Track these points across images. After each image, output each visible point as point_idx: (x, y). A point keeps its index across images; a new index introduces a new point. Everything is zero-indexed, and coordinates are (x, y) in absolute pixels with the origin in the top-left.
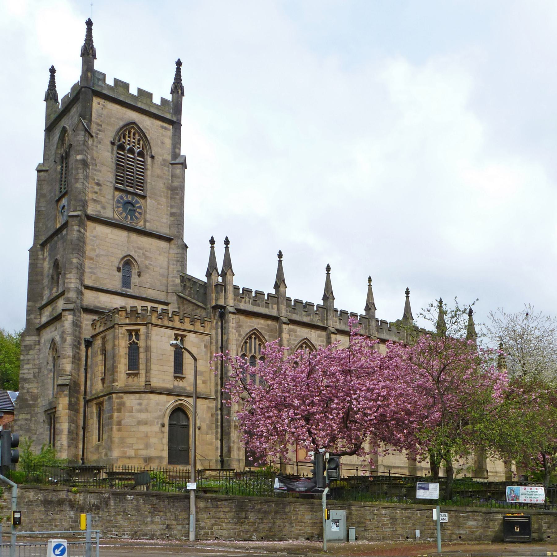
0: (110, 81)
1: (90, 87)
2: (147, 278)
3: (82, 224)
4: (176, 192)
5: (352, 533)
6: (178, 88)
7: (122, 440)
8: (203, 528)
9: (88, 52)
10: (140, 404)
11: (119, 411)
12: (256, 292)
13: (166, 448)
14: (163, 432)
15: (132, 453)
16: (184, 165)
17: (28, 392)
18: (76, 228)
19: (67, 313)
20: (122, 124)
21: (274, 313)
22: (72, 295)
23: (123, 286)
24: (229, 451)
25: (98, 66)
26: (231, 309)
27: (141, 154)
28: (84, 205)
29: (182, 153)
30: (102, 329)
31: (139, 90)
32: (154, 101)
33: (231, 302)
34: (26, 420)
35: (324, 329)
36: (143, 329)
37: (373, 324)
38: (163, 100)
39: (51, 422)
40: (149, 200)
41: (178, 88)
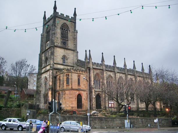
0: (60, 14)
1: (56, 15)
2: (69, 61)
3: (54, 48)
4: (75, 39)
5: (132, 126)
6: (75, 14)
7: (65, 102)
8: (92, 125)
9: (55, 8)
10: (70, 93)
11: (65, 95)
12: (97, 63)
13: (76, 104)
14: (76, 100)
15: (68, 106)
16: (77, 32)
17: (39, 90)
18: (52, 49)
19: (50, 70)
20: (62, 23)
21: (102, 68)
22: (52, 65)
23: (63, 63)
24: (92, 105)
25: (57, 11)
26: (92, 68)
27: (67, 30)
28: (54, 44)
29: (76, 30)
30: (59, 74)
31: (66, 15)
32: (70, 18)
33: (91, 66)
34: (38, 97)
35: (114, 72)
36: (70, 74)
37: (126, 70)
38: (72, 17)
39: (45, 98)
40: (69, 41)
41: (75, 14)
